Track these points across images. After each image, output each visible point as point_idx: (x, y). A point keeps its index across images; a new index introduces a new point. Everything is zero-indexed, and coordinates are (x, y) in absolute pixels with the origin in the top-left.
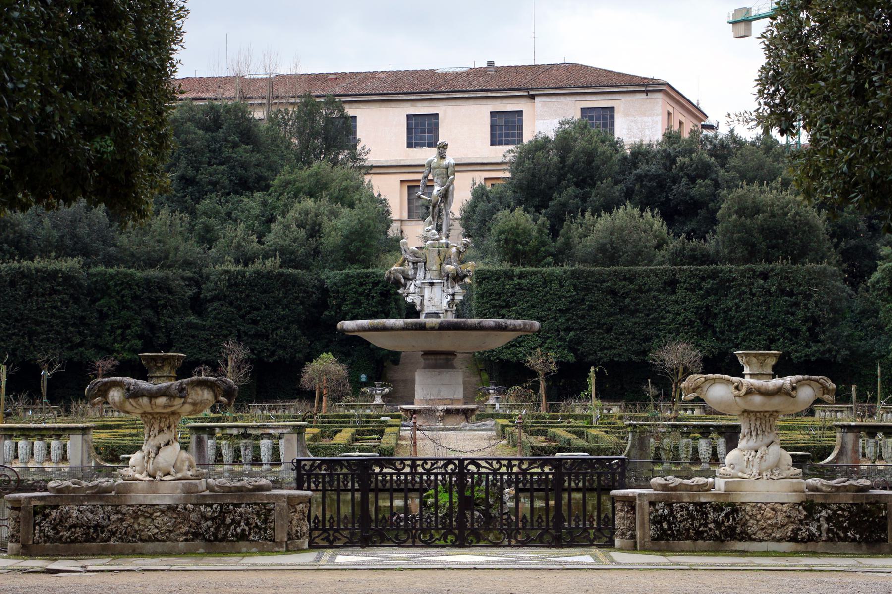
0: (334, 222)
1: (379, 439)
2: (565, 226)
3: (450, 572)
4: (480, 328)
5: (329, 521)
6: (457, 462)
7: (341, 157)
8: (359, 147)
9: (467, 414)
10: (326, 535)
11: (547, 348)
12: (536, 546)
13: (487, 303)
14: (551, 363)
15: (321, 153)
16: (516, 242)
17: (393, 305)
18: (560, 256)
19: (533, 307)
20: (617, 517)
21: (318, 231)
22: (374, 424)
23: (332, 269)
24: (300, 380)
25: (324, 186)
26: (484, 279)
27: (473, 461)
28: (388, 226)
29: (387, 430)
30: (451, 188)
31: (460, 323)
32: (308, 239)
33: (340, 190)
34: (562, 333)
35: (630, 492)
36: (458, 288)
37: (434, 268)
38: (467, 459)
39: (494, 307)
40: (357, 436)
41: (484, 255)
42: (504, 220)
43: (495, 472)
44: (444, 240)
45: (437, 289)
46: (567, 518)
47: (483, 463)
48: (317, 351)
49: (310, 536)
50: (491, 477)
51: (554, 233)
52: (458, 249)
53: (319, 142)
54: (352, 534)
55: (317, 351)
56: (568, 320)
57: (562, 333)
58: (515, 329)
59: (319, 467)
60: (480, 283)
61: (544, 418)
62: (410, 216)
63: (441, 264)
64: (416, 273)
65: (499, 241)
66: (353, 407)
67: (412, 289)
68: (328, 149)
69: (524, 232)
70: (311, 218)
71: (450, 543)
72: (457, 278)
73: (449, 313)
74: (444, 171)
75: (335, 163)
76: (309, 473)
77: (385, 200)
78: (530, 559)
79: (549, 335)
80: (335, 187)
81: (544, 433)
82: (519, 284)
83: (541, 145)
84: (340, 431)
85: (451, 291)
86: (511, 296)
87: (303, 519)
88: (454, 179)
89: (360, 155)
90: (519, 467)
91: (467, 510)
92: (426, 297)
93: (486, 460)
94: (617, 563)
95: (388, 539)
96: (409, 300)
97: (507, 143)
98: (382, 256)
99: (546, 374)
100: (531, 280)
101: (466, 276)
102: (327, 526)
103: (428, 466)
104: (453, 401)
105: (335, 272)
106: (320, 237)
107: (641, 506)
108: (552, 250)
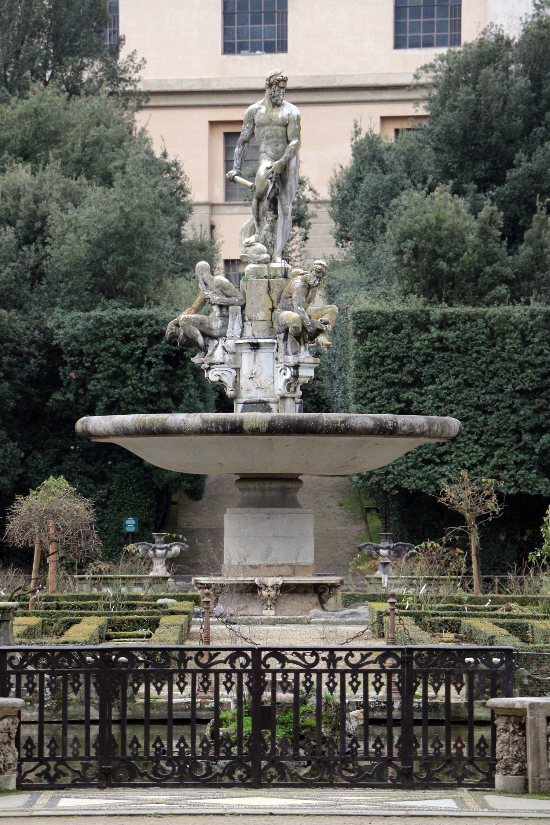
0: (72, 213)
1: (149, 636)
2: (535, 224)
3: (231, 818)
4: (346, 430)
6: (249, 653)
7: (86, 75)
8: (123, 55)
9: (320, 592)
10: (44, 767)
11: (494, 467)
12: (373, 787)
13: (376, 377)
14: (488, 497)
15: (45, 67)
16: (435, 256)
17: (190, 380)
18: (524, 284)
19: (468, 384)
20: (498, 742)
21: (41, 231)
22: (142, 610)
23: (69, 308)
24: (4, 528)
25: (52, 139)
26: (370, 329)
27: (275, 652)
28: (182, 219)
29: (165, 620)
30: (293, 163)
31: (307, 421)
32: (19, 247)
33: (84, 146)
34: (526, 437)
35: (518, 701)
36: (305, 355)
37: (261, 315)
38: (265, 649)
39: (391, 384)
40: (110, 632)
41: (375, 275)
42: (413, 210)
43: (308, 669)
44: (279, 263)
45: (265, 356)
47: (289, 655)
48: (39, 472)
49: (19, 769)
51: (514, 234)
52: (305, 281)
53: (41, 44)
54: (86, 767)
55: (39, 472)
56: (537, 412)
57: (526, 437)
58: (411, 434)
60: (362, 338)
61: (460, 601)
62: (228, 196)
63: (273, 309)
64: (225, 326)
65: (400, 253)
66: (106, 581)
67: (218, 355)
68: (59, 60)
69: (452, 236)
70: (26, 205)
72: (305, 335)
73: (289, 402)
74: (280, 130)
75: (74, 90)
77: (176, 164)
78: (359, 802)
79: (499, 440)
80: (73, 140)
81: (454, 627)
82: (440, 339)
83: (492, 52)
84: (79, 621)
85: (291, 360)
86: (425, 362)
87: (9, 743)
88: (298, 146)
89: (125, 71)
90: (347, 662)
92: (245, 371)
94: (491, 809)
95: (142, 775)
96: (212, 376)
97: (428, 44)
98: (168, 282)
99: (479, 519)
100: (464, 332)
101: (319, 331)
102: (47, 753)
103: (204, 660)
104: (294, 569)
105: (75, 314)
106: (44, 244)
107: (535, 726)
108: (508, 271)
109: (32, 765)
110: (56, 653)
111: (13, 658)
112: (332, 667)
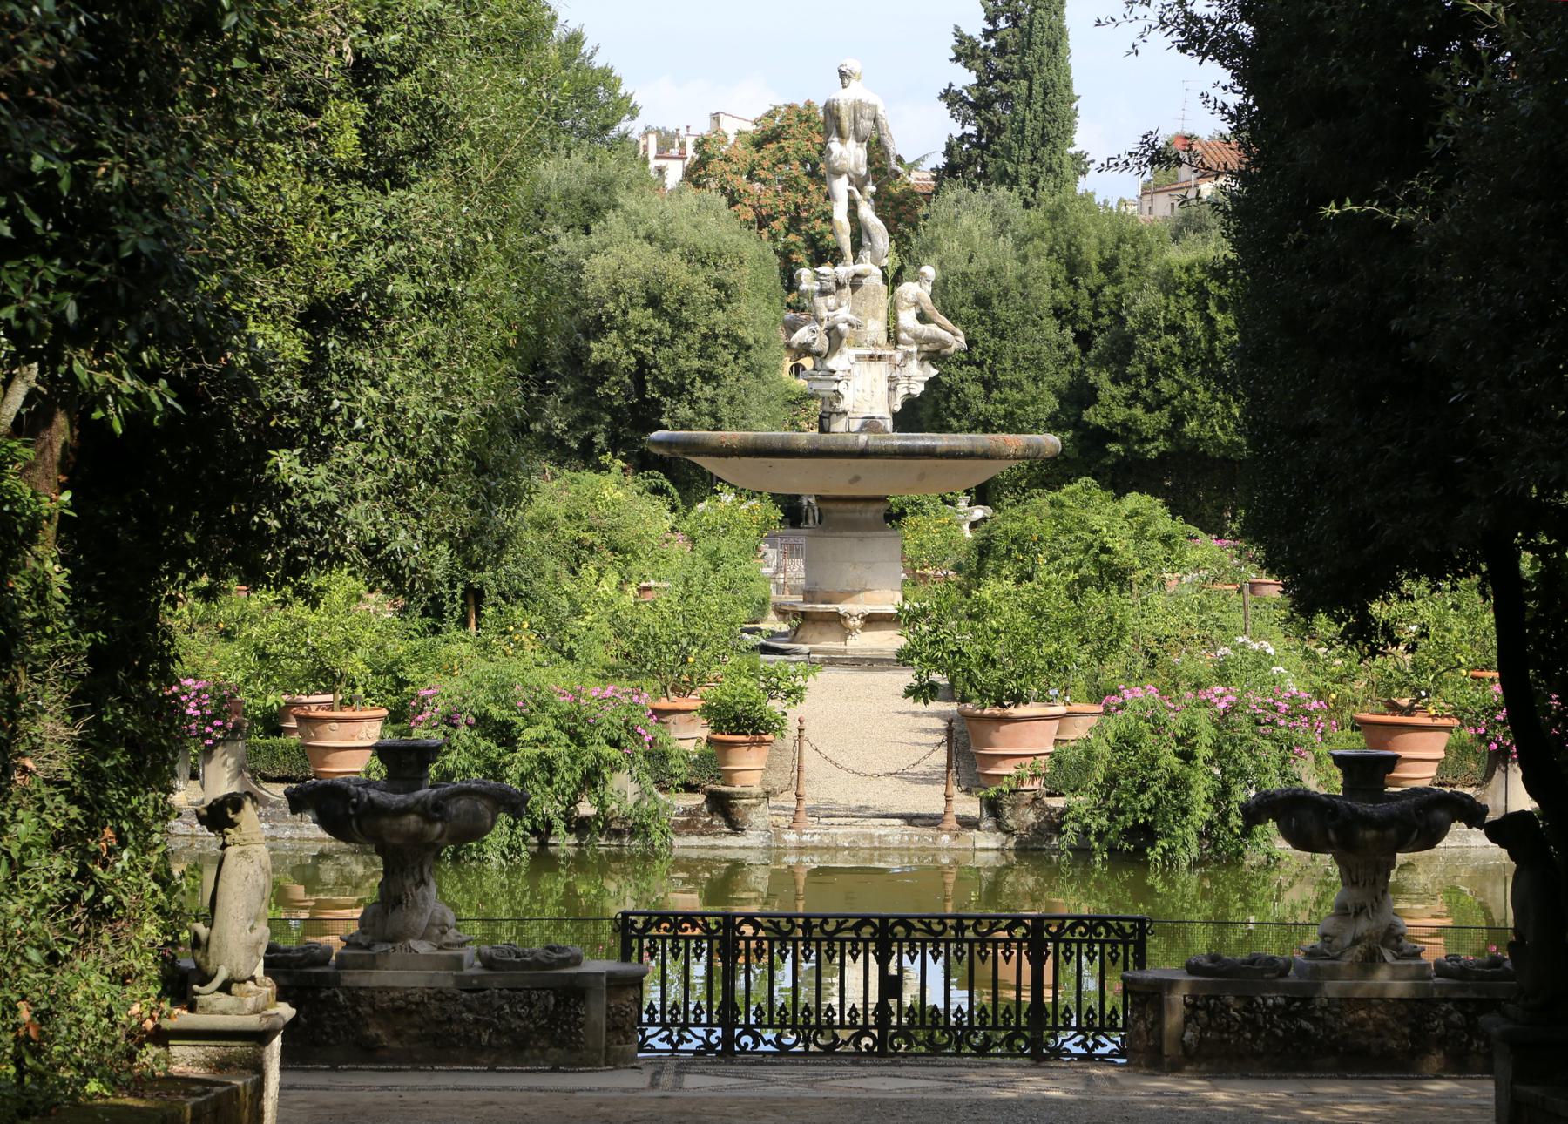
5: (1063, 1016)
6: (877, 922)
10: (666, 1033)
46: (742, 1010)
47: (915, 923)
59: (1072, 929)
90: (975, 931)
109: (657, 1029)
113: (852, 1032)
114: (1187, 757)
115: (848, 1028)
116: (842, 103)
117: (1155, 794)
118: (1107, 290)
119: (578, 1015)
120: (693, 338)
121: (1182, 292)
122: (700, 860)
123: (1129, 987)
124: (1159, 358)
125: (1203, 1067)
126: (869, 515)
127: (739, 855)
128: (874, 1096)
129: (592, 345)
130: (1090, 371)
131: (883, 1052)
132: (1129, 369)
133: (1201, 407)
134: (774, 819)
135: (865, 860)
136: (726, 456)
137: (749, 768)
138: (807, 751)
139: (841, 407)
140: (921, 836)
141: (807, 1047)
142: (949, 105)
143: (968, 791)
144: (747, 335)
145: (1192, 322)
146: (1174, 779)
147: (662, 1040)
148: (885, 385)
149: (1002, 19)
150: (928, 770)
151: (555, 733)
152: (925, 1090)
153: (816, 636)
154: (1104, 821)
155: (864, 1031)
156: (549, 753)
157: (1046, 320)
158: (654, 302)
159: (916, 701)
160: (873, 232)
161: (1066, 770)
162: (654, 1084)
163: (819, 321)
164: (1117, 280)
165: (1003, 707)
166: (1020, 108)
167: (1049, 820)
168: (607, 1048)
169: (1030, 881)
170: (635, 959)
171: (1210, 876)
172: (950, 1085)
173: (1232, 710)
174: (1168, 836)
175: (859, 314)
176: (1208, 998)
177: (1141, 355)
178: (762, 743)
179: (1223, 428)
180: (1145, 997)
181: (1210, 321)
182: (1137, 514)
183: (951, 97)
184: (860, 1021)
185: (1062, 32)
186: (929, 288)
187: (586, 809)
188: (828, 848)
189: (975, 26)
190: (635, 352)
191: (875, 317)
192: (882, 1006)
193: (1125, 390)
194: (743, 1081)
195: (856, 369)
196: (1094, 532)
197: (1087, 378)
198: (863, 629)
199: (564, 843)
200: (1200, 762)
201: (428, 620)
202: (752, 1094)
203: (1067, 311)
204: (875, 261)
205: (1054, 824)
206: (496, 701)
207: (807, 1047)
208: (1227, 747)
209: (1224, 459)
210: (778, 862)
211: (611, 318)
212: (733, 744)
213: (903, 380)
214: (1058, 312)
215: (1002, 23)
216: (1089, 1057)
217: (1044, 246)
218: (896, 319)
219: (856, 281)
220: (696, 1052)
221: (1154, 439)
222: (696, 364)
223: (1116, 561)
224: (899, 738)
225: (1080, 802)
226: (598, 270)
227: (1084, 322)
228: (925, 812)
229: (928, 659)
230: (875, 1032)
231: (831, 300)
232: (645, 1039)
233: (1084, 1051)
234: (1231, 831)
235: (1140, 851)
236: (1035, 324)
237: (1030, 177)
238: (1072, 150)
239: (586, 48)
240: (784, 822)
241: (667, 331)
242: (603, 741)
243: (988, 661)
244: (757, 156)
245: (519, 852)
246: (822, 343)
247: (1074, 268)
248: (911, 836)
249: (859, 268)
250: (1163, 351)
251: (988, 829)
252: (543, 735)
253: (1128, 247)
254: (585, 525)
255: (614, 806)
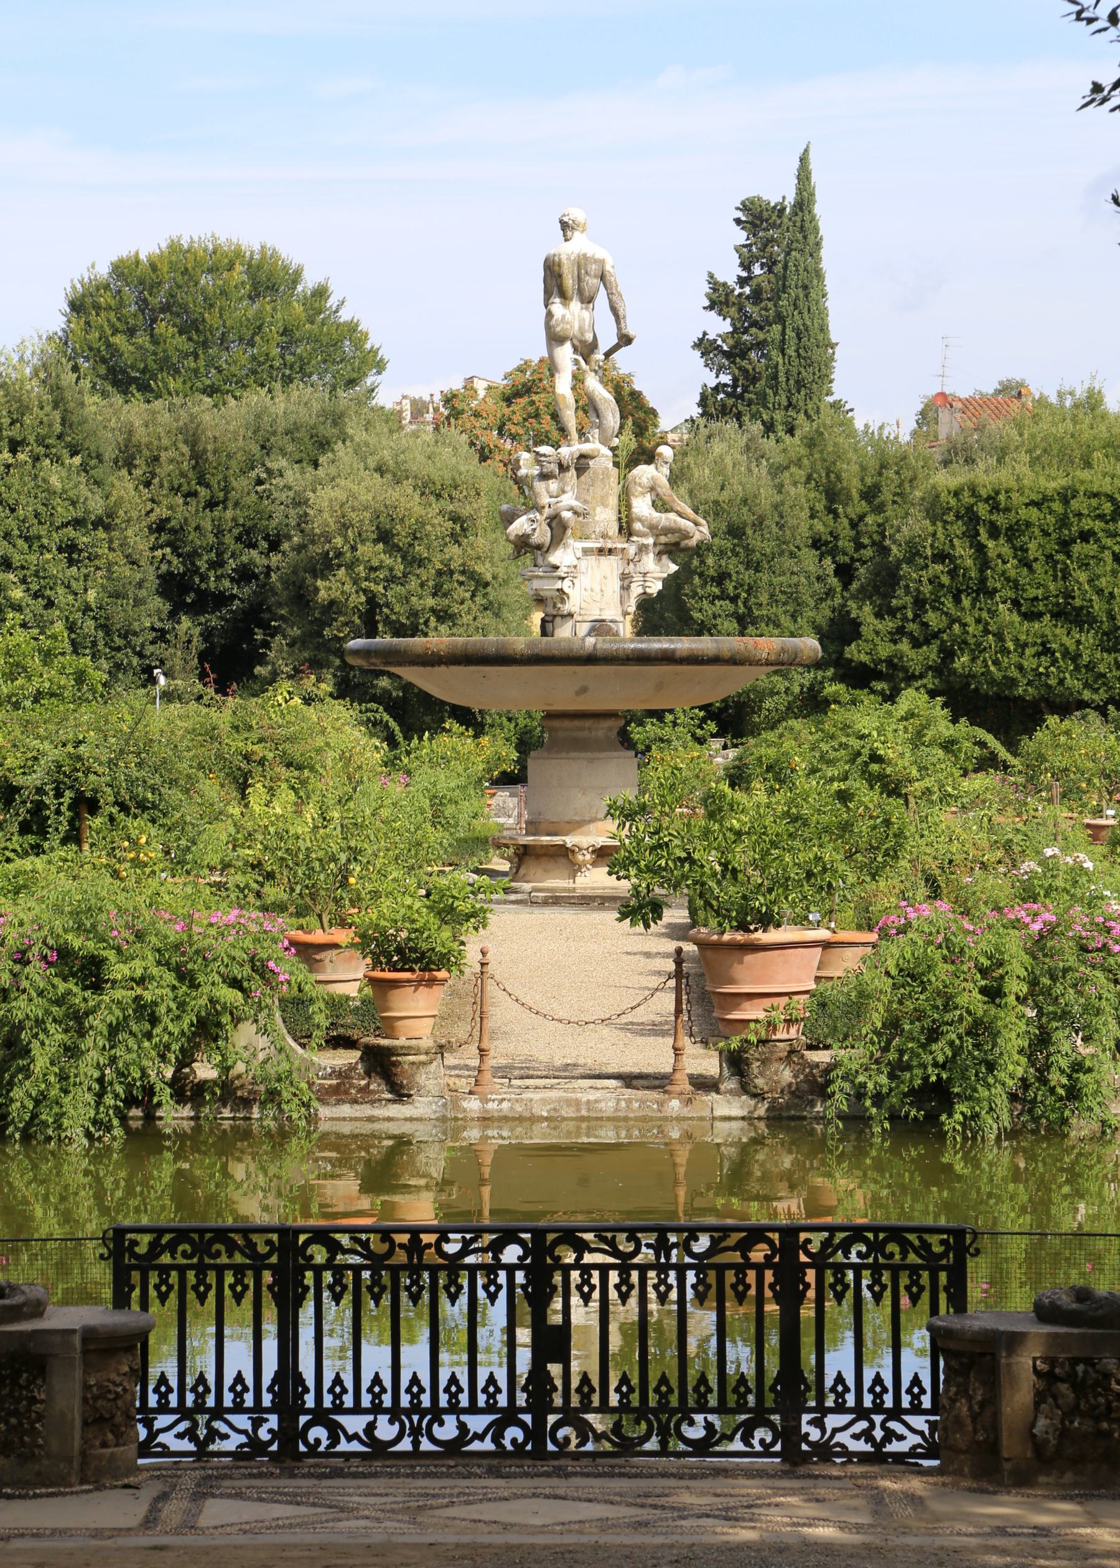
10: (863, 1425)
47: (345, 1240)
50: (366, 1275)
59: (845, 1247)
71: (758, 1448)
76: (146, 1264)
91: (554, 1361)
93: (351, 1230)
109: (173, 1418)
110: (208, 1236)
111: (135, 1243)
112: (663, 1260)
113: (491, 1418)
114: (993, 993)
115: (482, 1411)
116: (564, 257)
117: (951, 1043)
118: (869, 520)
119: (33, 1400)
120: (427, 574)
121: (950, 517)
122: (354, 1136)
123: (941, 1344)
124: (927, 589)
125: (1068, 1477)
126: (600, 734)
127: (407, 1128)
128: (514, 1539)
129: (319, 583)
130: (852, 604)
131: (536, 1452)
132: (894, 602)
133: (972, 641)
134: (451, 1081)
135: (569, 1133)
136: (433, 665)
137: (418, 1013)
138: (491, 987)
139: (567, 608)
140: (642, 1102)
141: (416, 1443)
142: (703, 355)
143: (705, 1043)
144: (485, 570)
145: (963, 551)
146: (977, 1022)
147: (180, 1436)
148: (616, 584)
149: (757, 265)
150: (658, 1019)
151: (155, 971)
152: (604, 1525)
153: (540, 872)
154: (883, 1079)
155: (509, 1416)
156: (148, 996)
157: (805, 550)
158: (384, 537)
159: (633, 924)
160: (602, 407)
161: (832, 1015)
162: (150, 1521)
163: (540, 509)
164: (879, 509)
165: (748, 931)
166: (774, 353)
167: (811, 1081)
168: (83, 1454)
169: (787, 1162)
170: (135, 1307)
171: (1024, 1150)
172: (644, 1514)
173: (1052, 932)
174: (970, 1098)
175: (586, 502)
176: (1074, 1361)
177: (907, 587)
178: (432, 982)
179: (996, 663)
180: (970, 1359)
181: (981, 549)
182: (913, 715)
183: (705, 346)
184: (502, 1400)
185: (819, 275)
186: (666, 470)
187: (205, 1071)
188: (520, 1119)
189: (730, 272)
190: (365, 591)
191: (605, 505)
192: (539, 1377)
193: (890, 624)
194: (303, 1510)
195: (583, 565)
196: (862, 737)
197: (848, 613)
198: (594, 864)
199: (174, 1116)
200: (1011, 999)
201: (31, 839)
202: (309, 1538)
203: (827, 543)
204: (604, 441)
205: (817, 1085)
206: (79, 928)
207: (416, 1443)
208: (1046, 981)
209: (998, 697)
210: (455, 1138)
211: (339, 554)
212: (395, 984)
213: (638, 578)
214: (816, 543)
215: (757, 270)
216: (877, 1457)
217: (800, 474)
218: (629, 507)
219: (582, 463)
220: (236, 1455)
221: (921, 676)
222: (430, 602)
223: (889, 770)
224: (626, 982)
225: (850, 1056)
226: (325, 503)
227: (845, 554)
228: (650, 1070)
229: (649, 869)
230: (527, 1418)
231: (553, 485)
232: (152, 1435)
233: (868, 1448)
234: (1052, 1091)
235: (932, 1118)
236: (792, 555)
237: (785, 423)
238: (830, 399)
239: (332, 302)
240: (463, 1084)
241: (399, 569)
242: (218, 979)
243: (730, 871)
244: (507, 411)
245: (109, 1129)
246: (542, 535)
247: (833, 496)
248: (629, 1101)
249: (586, 448)
250: (930, 582)
251: (731, 1092)
252: (139, 973)
253: (891, 474)
254: (254, 736)
255: (240, 1068)
